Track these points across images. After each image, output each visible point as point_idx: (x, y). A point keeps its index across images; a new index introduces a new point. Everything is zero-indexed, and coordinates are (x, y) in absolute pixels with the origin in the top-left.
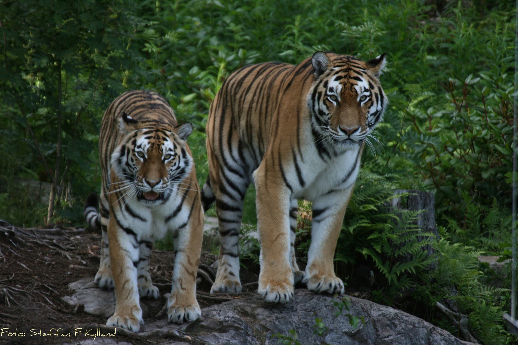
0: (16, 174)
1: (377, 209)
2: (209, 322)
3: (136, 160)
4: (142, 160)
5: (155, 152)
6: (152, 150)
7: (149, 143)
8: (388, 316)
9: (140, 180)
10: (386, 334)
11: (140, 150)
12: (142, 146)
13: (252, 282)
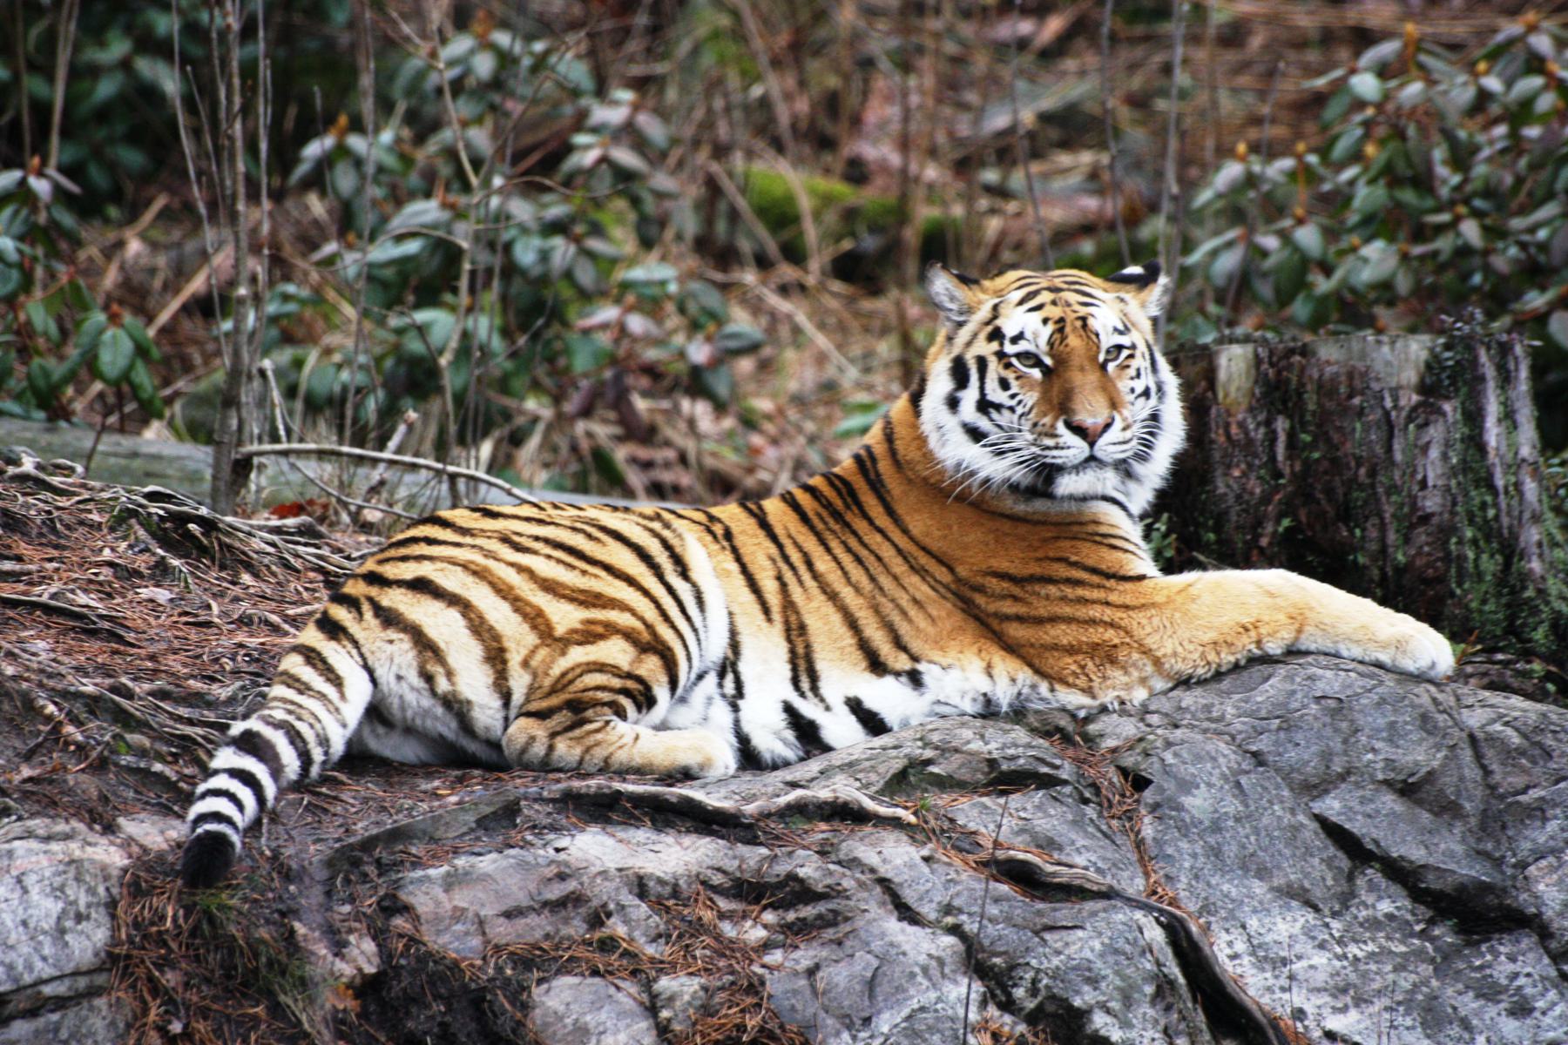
2: (955, 766)
3: (1018, 378)
4: (1036, 373)
5: (1074, 341)
6: (1064, 338)
7: (1045, 321)
8: (1517, 724)
10: (1519, 781)
11: (1023, 346)
12: (1028, 335)
13: (113, 701)
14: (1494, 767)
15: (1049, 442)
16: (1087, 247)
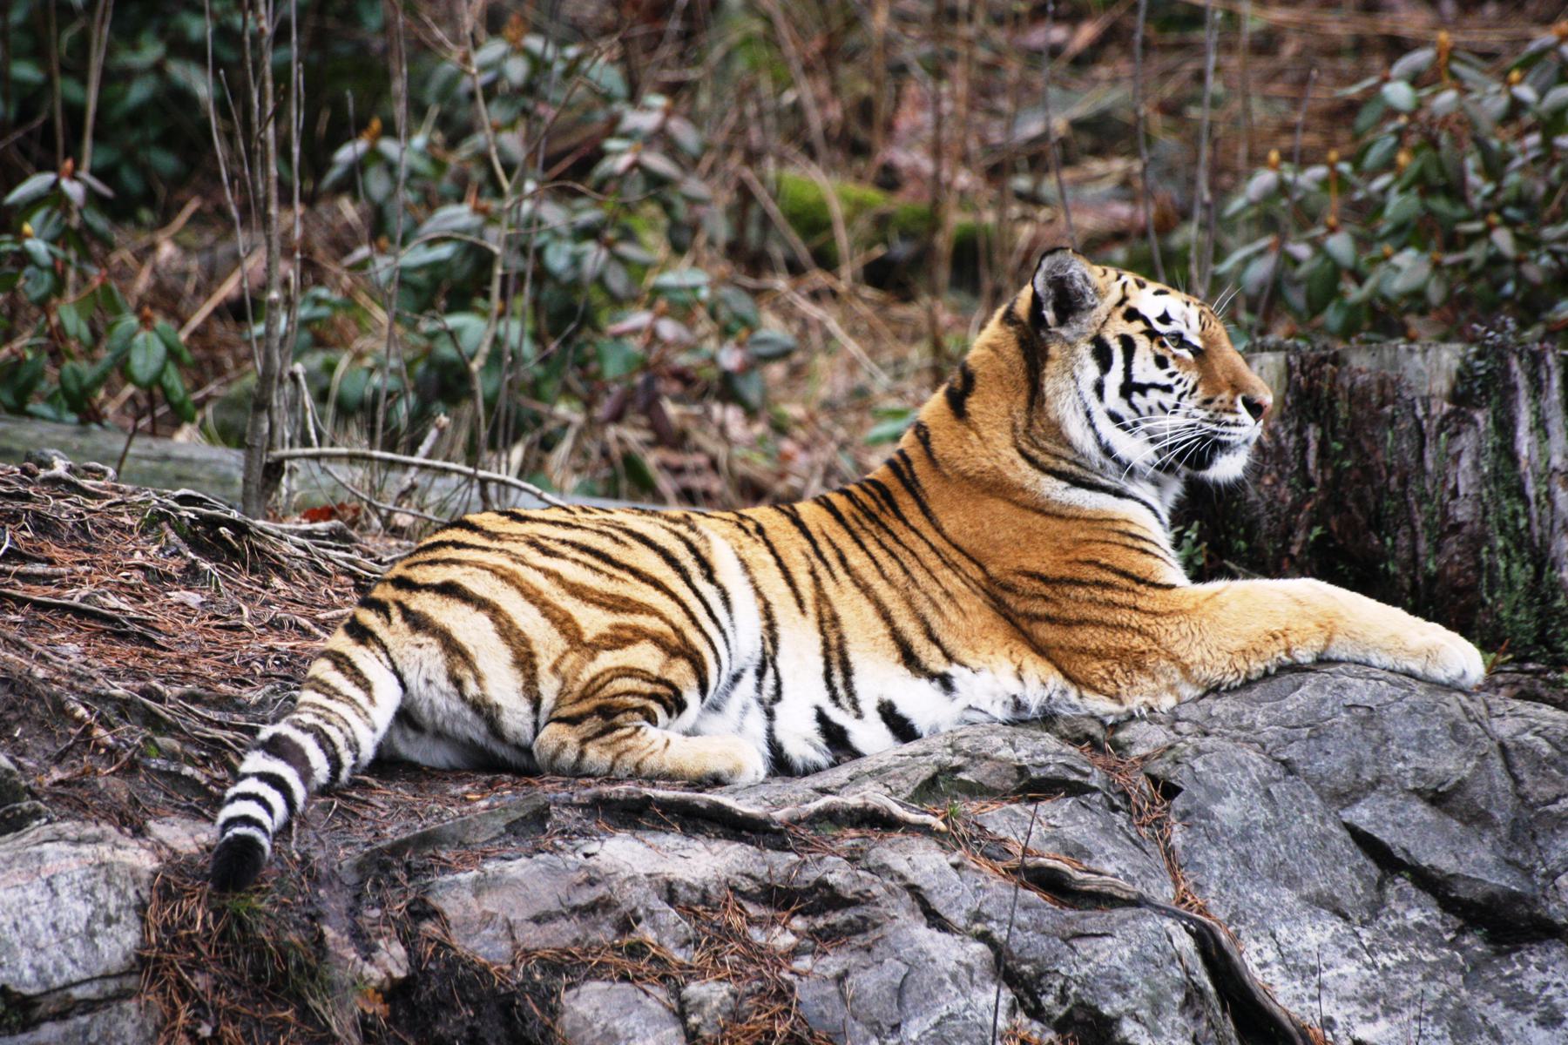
0: (42, 950)
1: (13, 207)
8: (1548, 733)
9: (1226, 405)
10: (1549, 791)
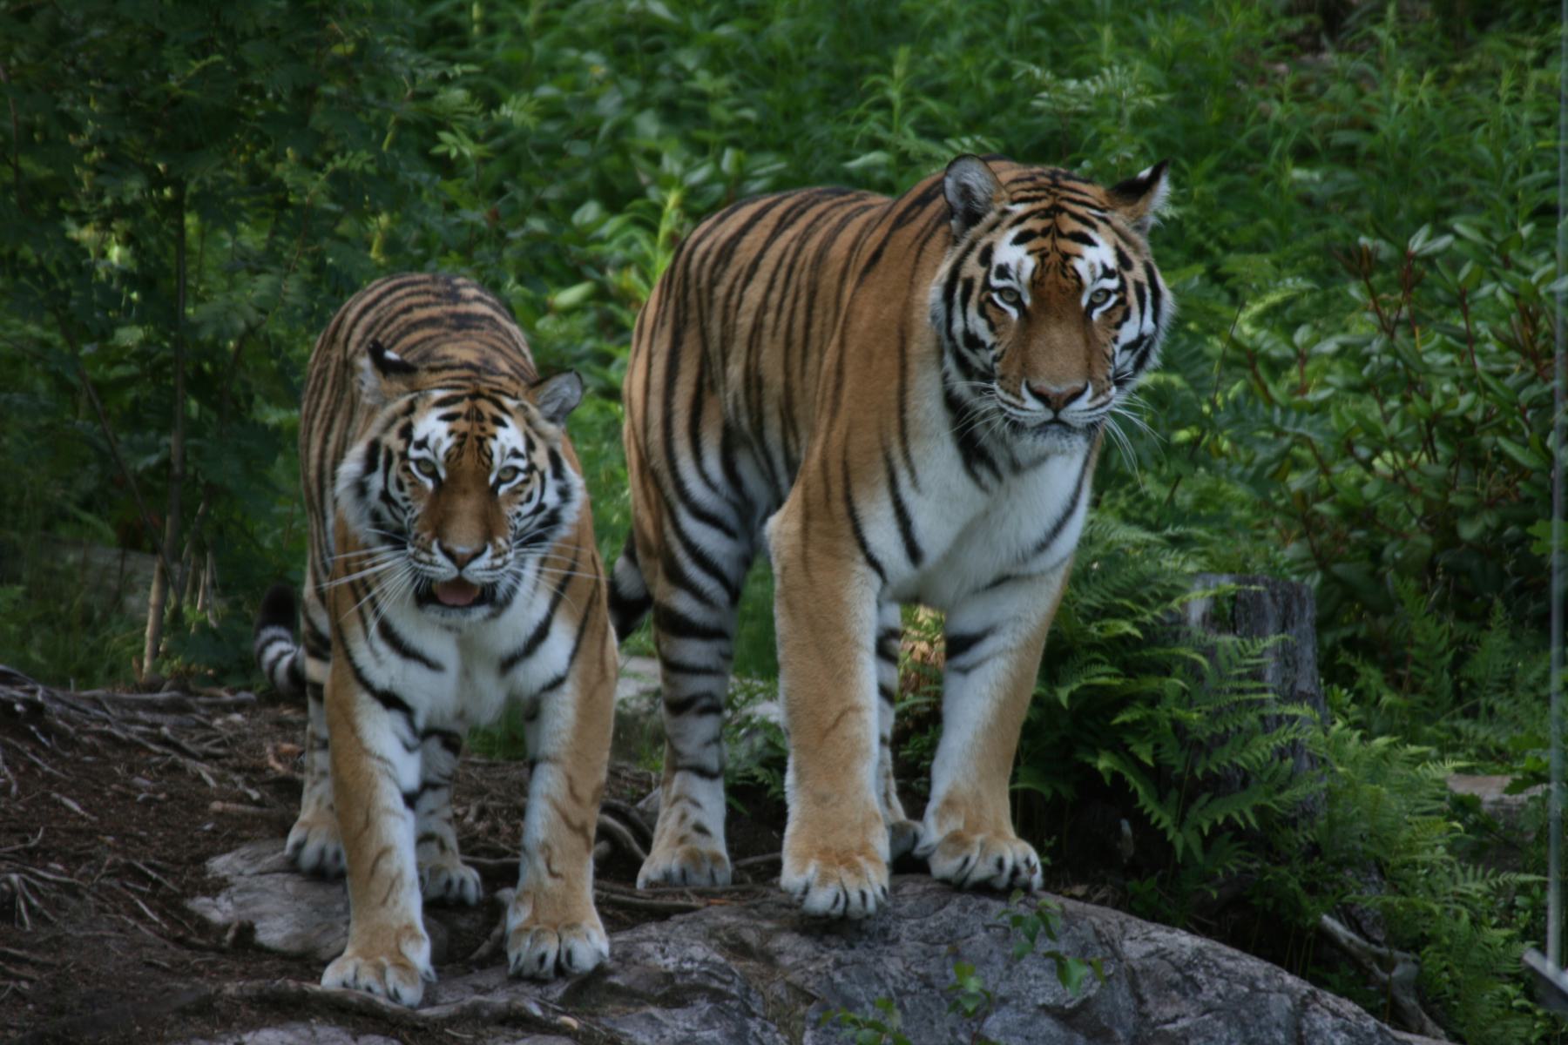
3: (412, 484)
4: (429, 484)
6: (460, 455)
7: (451, 433)
8: (1173, 958)
10: (1169, 1011)
11: (424, 453)
12: (431, 443)
14: (1148, 996)
15: (424, 557)
16: (1270, 470)
